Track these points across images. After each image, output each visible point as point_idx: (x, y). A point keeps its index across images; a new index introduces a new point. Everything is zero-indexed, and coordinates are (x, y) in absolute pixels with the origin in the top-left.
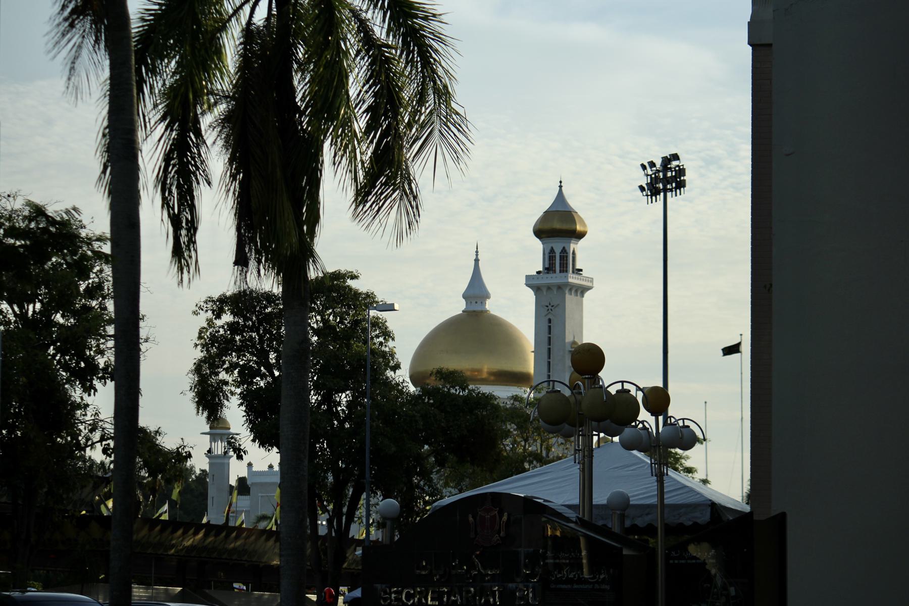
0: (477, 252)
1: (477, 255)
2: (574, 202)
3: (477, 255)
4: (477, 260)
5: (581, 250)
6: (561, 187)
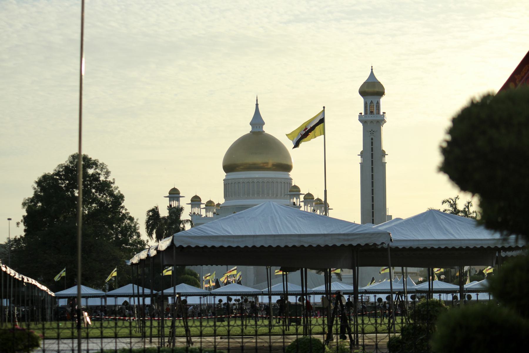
0: (257, 100)
2: (380, 78)
4: (257, 105)
5: (385, 104)
6: (372, 69)
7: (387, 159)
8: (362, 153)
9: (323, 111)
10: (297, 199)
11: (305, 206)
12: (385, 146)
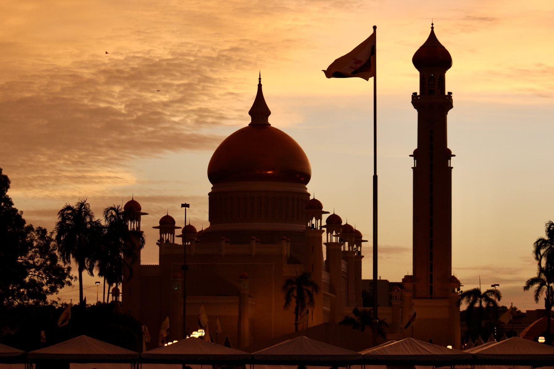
0: (260, 79)
1: (260, 81)
2: (442, 39)
3: (260, 81)
4: (260, 86)
5: (453, 81)
6: (432, 28)
7: (453, 162)
8: (415, 152)
9: (373, 38)
10: (317, 219)
11: (327, 233)
12: (453, 142)
